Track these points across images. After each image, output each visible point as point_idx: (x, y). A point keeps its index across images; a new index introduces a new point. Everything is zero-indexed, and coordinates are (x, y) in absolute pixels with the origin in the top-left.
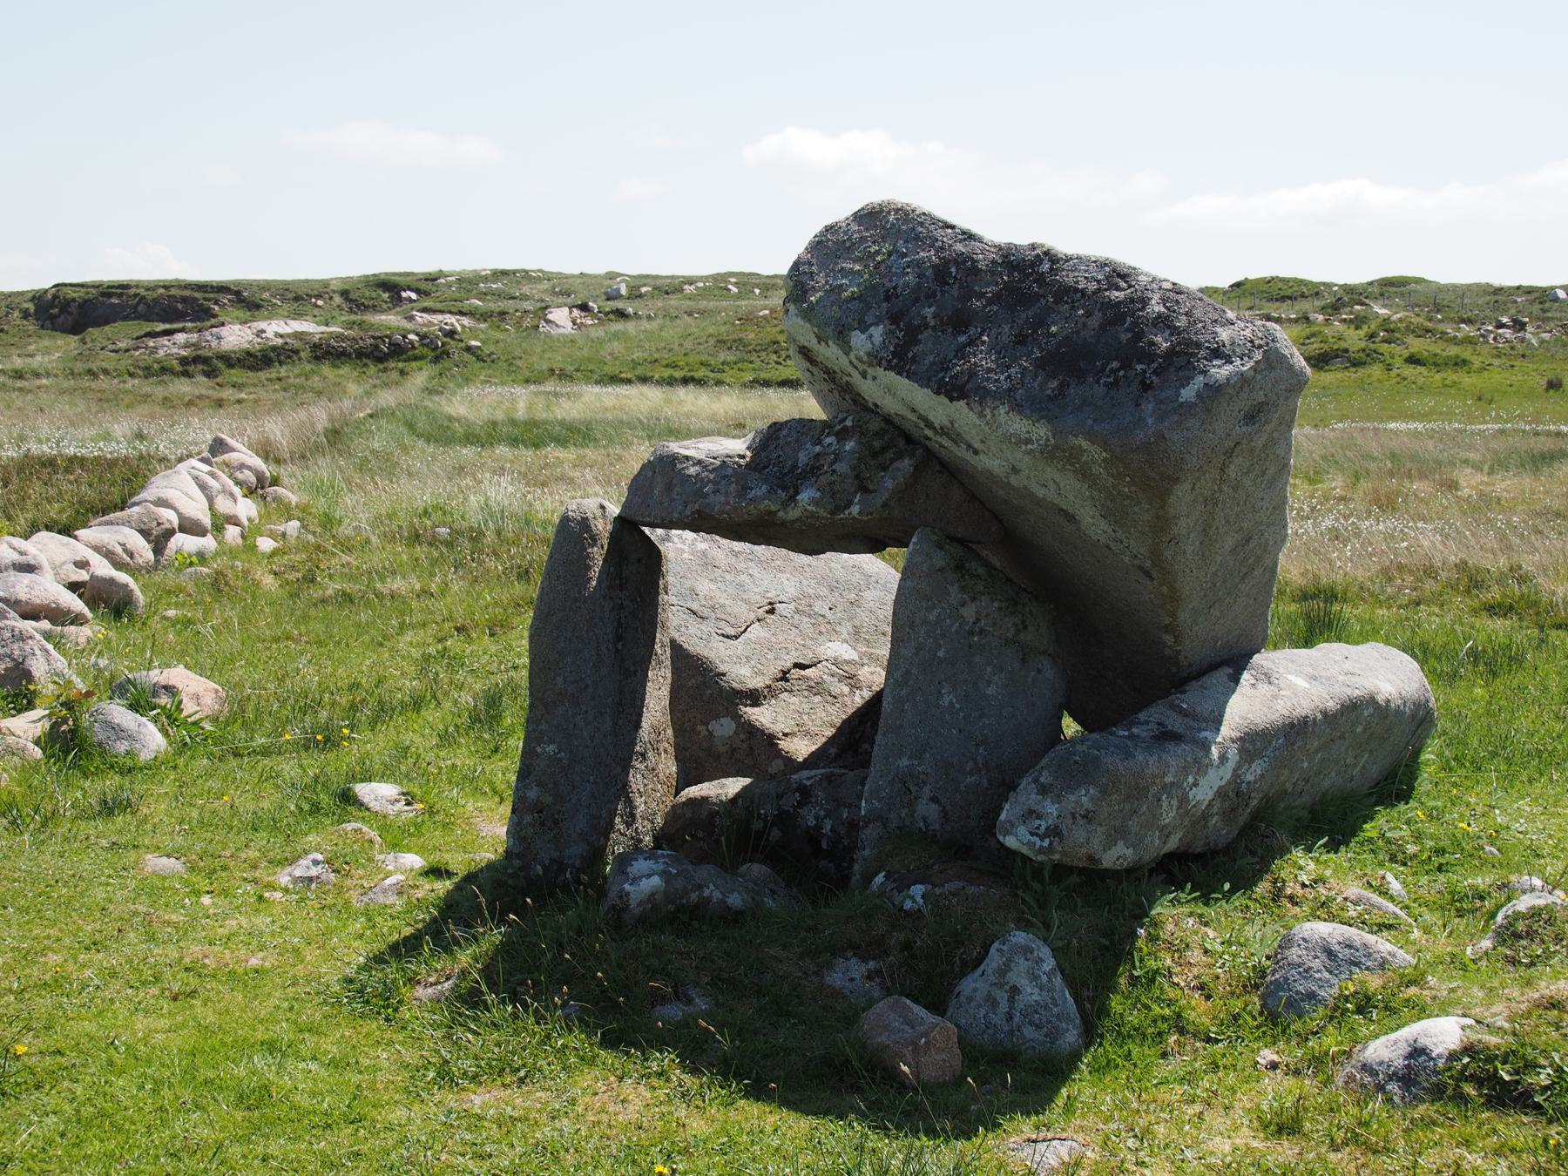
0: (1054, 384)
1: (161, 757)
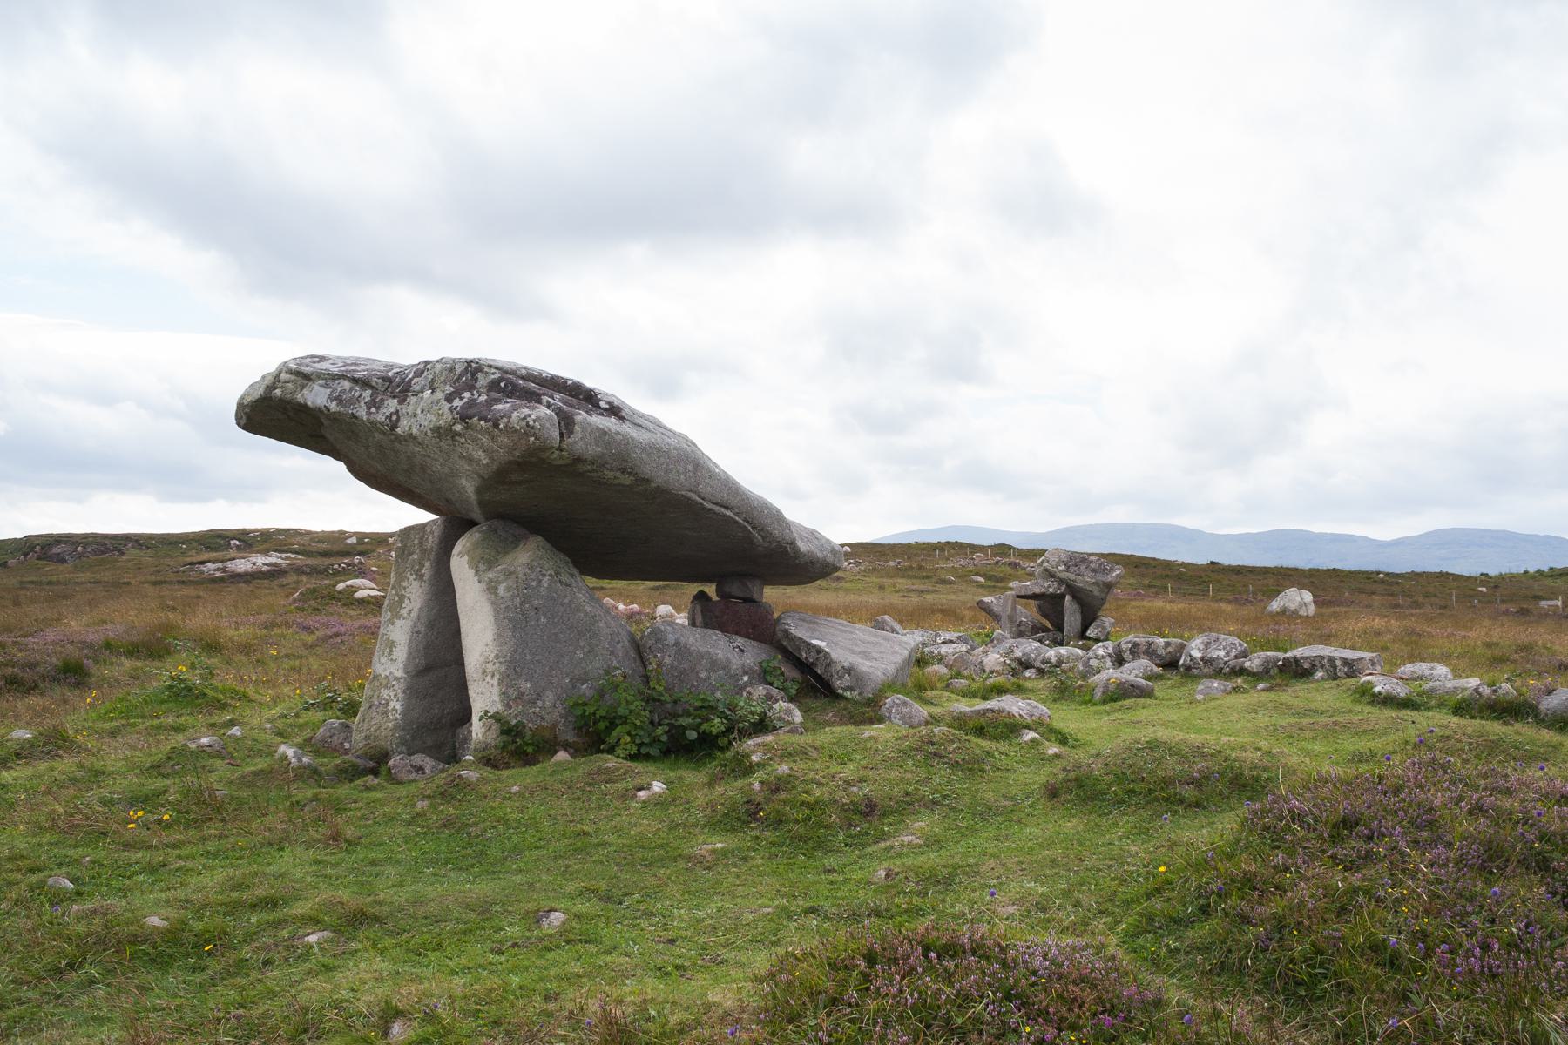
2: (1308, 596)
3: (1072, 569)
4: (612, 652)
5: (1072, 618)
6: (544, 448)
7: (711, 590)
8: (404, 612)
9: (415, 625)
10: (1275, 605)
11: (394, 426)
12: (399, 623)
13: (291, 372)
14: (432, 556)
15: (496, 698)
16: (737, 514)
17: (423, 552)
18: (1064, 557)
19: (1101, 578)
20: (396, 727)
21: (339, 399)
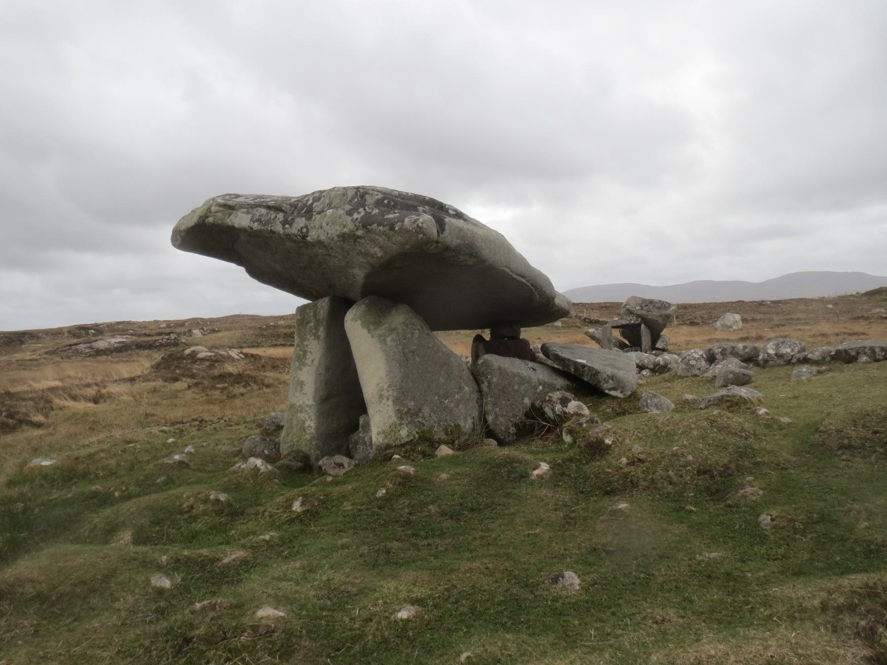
3: (645, 308)
4: (460, 377)
5: (646, 339)
6: (429, 241)
7: (487, 335)
8: (308, 361)
9: (317, 369)
11: (304, 237)
12: (305, 369)
13: (220, 205)
14: (325, 323)
15: (392, 413)
16: (528, 281)
17: (318, 321)
18: (639, 302)
19: (663, 312)
20: (313, 438)
21: (259, 220)
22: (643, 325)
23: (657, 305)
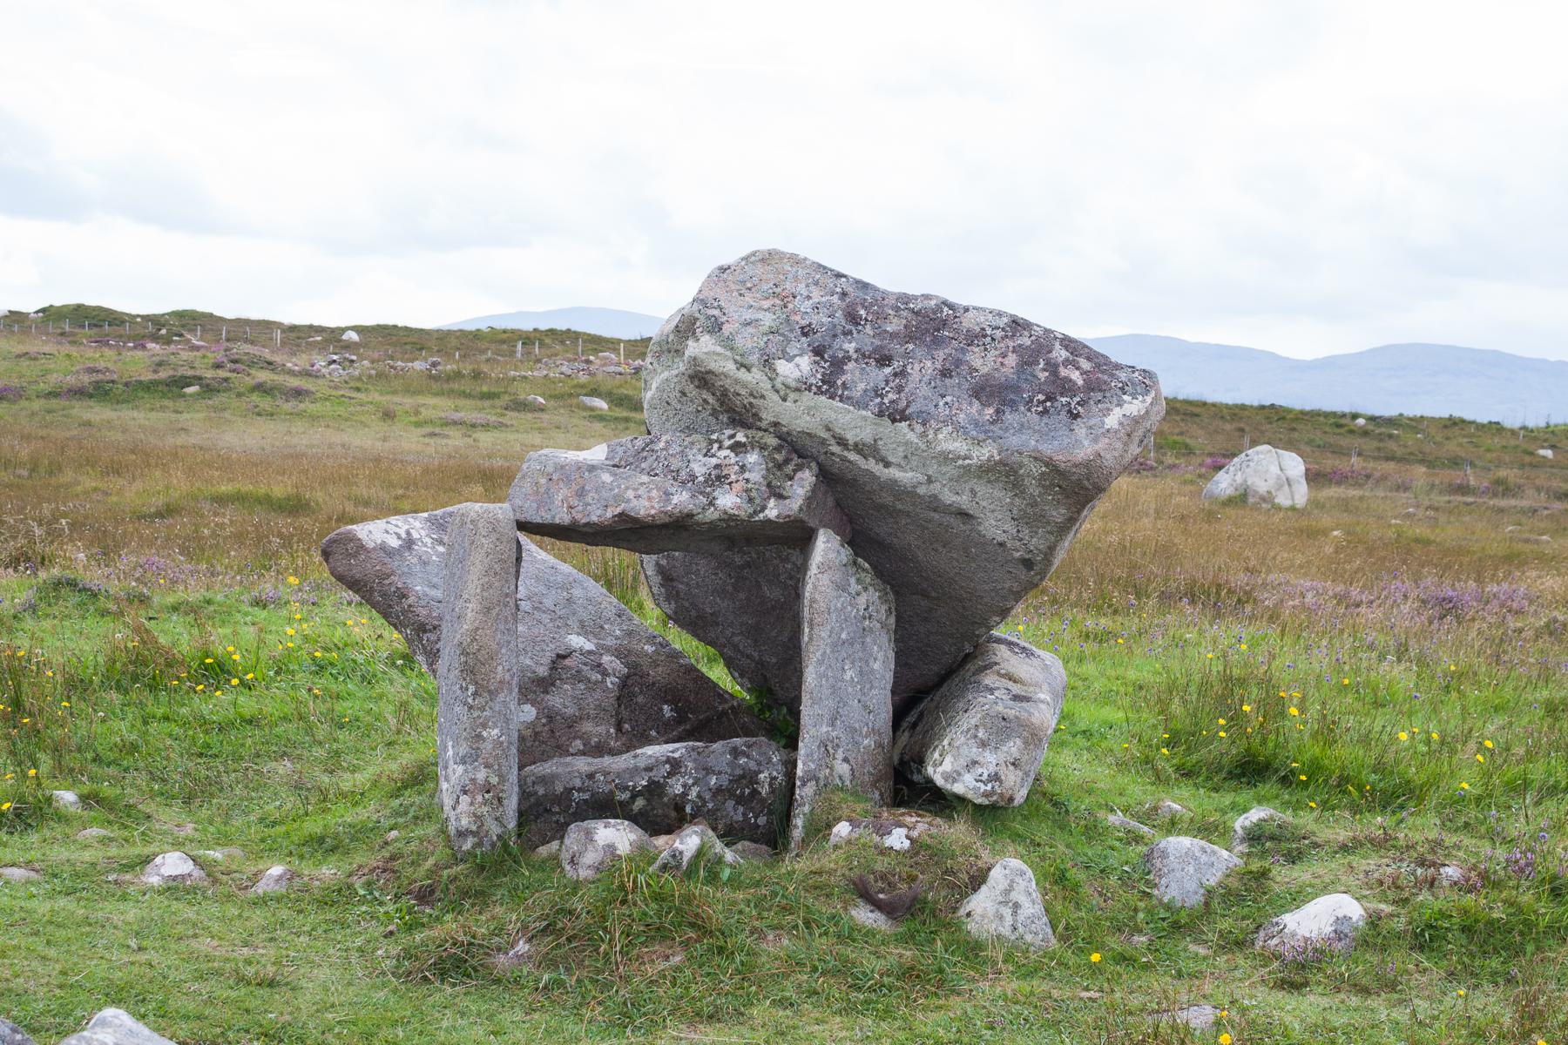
0: (991, 411)
1: (783, 742)
2: (1295, 465)
3: (859, 378)
10: (1224, 483)
18: (813, 306)
19: (1031, 437)
22: (826, 548)
23: (982, 362)
